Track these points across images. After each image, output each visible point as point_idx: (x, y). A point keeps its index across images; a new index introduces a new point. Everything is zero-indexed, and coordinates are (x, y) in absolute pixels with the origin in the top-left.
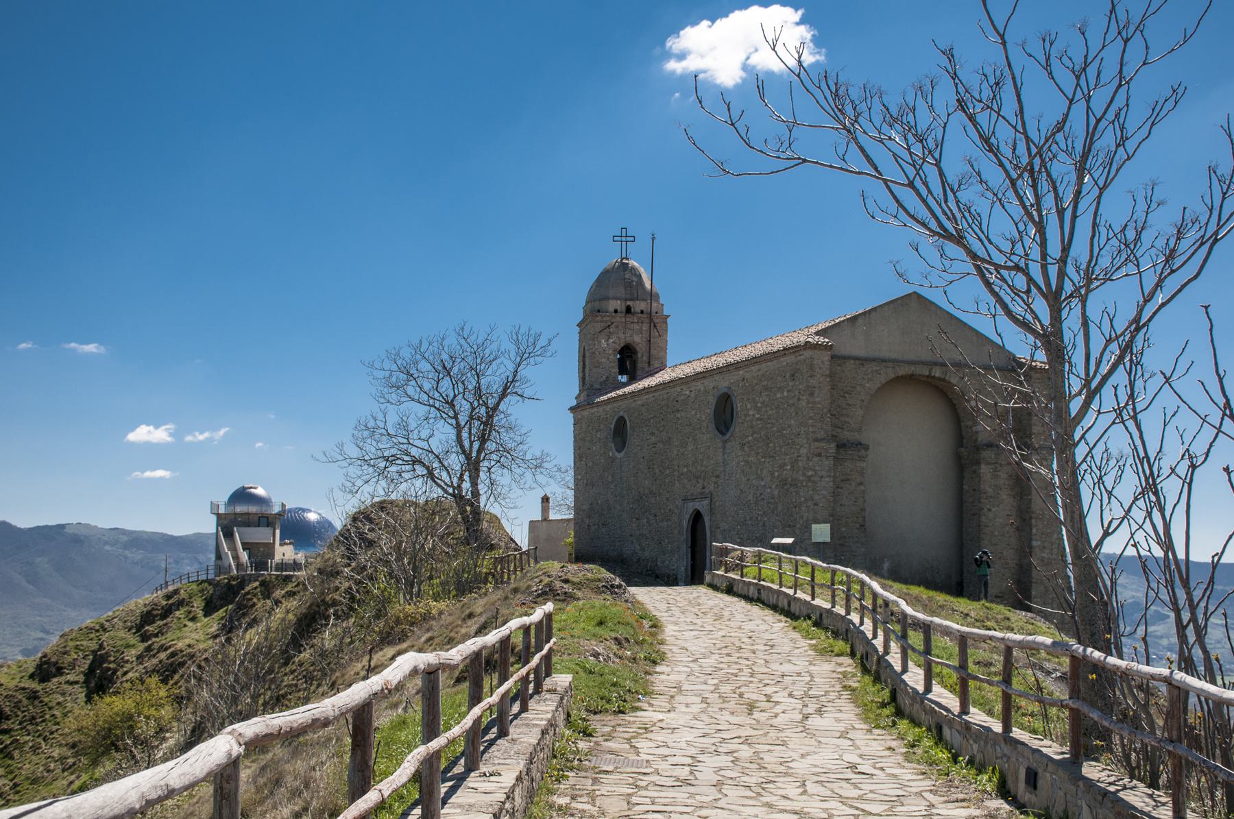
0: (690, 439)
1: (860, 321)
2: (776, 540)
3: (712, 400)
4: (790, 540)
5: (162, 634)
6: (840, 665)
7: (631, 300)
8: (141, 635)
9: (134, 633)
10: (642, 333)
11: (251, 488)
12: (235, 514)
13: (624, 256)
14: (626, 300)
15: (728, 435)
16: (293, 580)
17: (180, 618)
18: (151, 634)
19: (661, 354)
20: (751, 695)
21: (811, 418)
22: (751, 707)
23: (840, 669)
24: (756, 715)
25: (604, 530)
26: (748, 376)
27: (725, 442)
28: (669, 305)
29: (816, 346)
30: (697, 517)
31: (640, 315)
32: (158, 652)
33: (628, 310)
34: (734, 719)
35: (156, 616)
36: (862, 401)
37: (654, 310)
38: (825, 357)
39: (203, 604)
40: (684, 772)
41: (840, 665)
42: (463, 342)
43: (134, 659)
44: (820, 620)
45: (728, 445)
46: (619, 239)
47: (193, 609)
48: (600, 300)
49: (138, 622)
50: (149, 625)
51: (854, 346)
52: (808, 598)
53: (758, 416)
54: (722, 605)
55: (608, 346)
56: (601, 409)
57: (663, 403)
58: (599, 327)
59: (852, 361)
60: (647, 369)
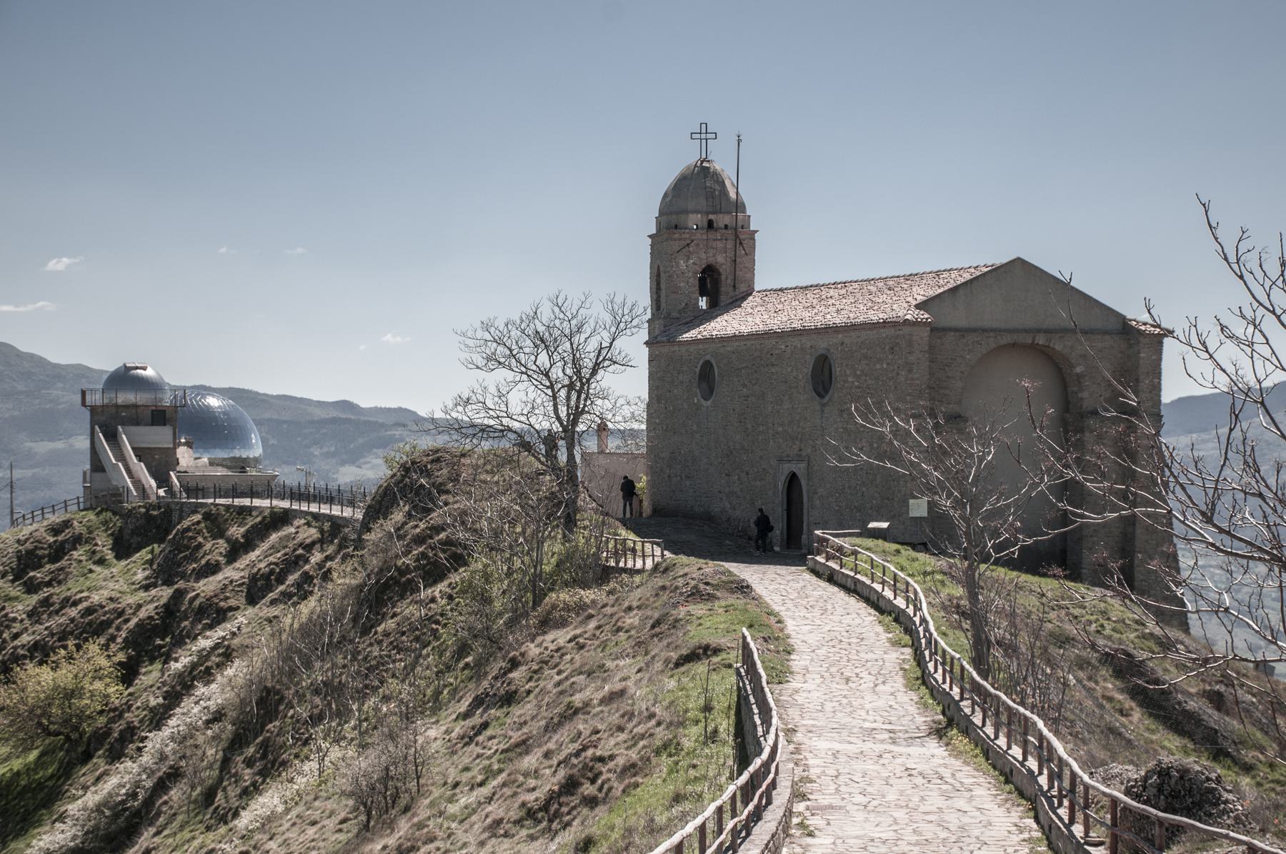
0: (787, 397)
1: (961, 292)
2: (872, 525)
3: (810, 361)
4: (885, 525)
5: (60, 583)
6: (903, 653)
7: (714, 213)
8: (25, 584)
9: (13, 581)
10: (726, 252)
11: (137, 368)
12: (117, 406)
13: (704, 156)
14: (708, 213)
15: (827, 398)
16: (254, 513)
17: (81, 561)
18: (41, 582)
19: (748, 275)
20: (847, 674)
21: (909, 394)
22: (848, 680)
23: (902, 657)
24: (850, 684)
25: (688, 483)
26: (847, 341)
27: (824, 405)
28: (758, 217)
29: (915, 324)
30: (793, 478)
31: (724, 231)
32: (62, 608)
33: (710, 225)
34: (838, 687)
35: (43, 557)
36: (962, 372)
37: (740, 224)
38: (926, 332)
39: (111, 542)
40: (820, 708)
41: (903, 653)
42: (556, 310)
43: (24, 616)
44: (899, 618)
45: (827, 409)
46: (698, 136)
47: (98, 548)
48: (678, 213)
49: (14, 565)
50: (33, 570)
51: (957, 317)
52: (892, 597)
53: (857, 384)
54: (825, 597)
55: (688, 268)
56: (683, 349)
57: (756, 354)
58: (676, 246)
59: (952, 333)
60: (731, 294)
